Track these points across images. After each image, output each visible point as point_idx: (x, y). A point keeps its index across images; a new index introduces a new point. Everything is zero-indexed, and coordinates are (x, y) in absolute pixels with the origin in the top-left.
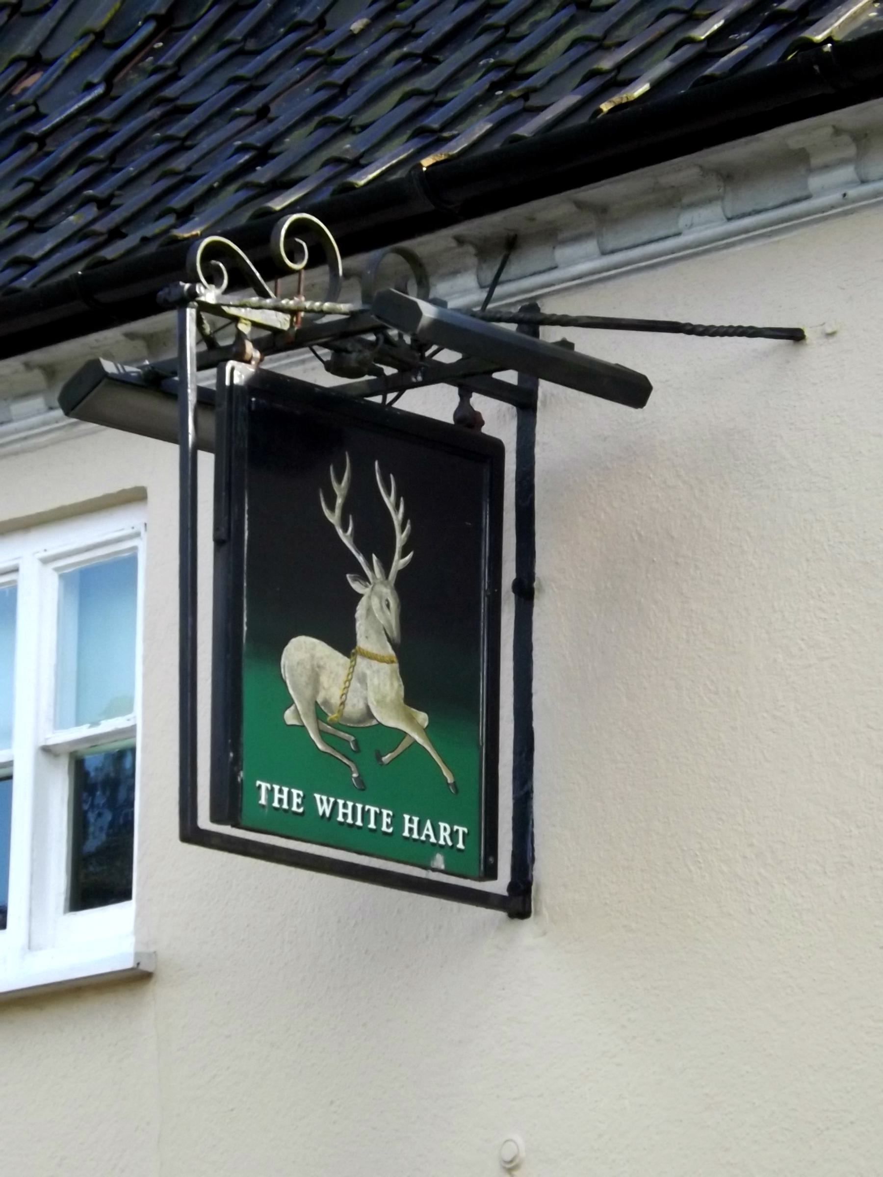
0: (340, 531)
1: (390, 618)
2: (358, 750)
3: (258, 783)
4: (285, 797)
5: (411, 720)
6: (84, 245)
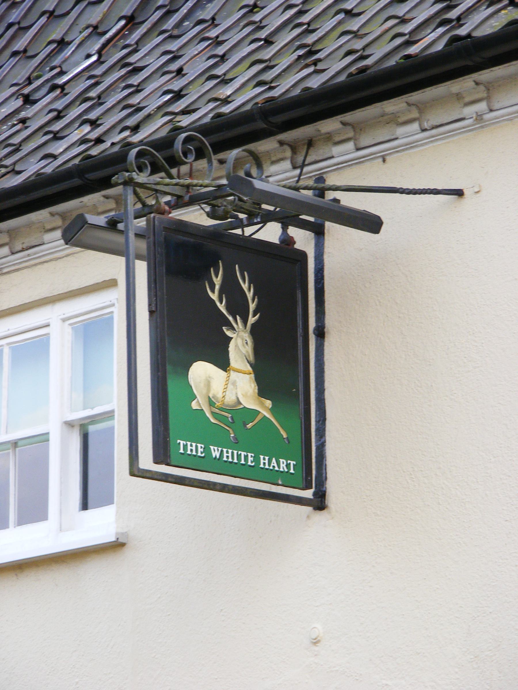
0: (218, 304)
1: (248, 349)
2: (233, 422)
3: (179, 441)
4: (194, 448)
5: (262, 405)
6: (83, 147)
